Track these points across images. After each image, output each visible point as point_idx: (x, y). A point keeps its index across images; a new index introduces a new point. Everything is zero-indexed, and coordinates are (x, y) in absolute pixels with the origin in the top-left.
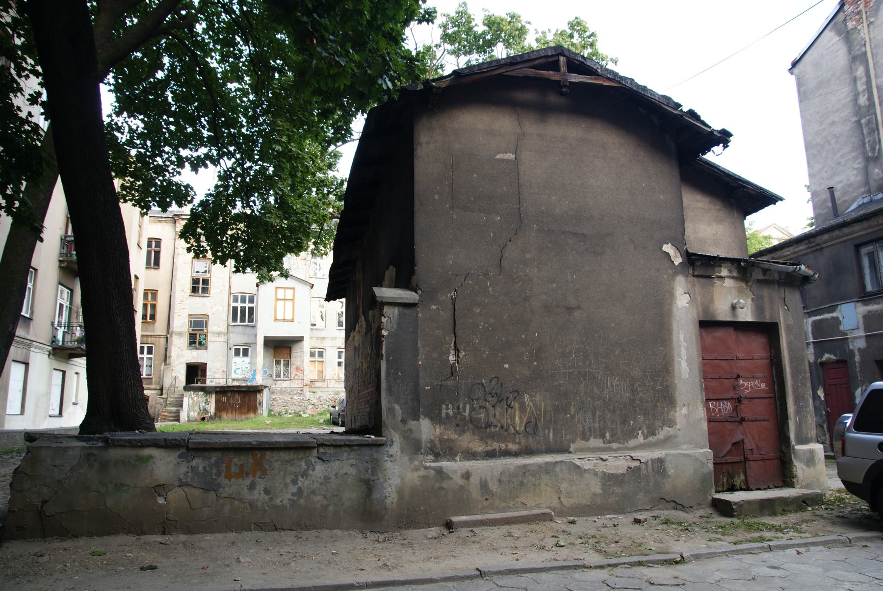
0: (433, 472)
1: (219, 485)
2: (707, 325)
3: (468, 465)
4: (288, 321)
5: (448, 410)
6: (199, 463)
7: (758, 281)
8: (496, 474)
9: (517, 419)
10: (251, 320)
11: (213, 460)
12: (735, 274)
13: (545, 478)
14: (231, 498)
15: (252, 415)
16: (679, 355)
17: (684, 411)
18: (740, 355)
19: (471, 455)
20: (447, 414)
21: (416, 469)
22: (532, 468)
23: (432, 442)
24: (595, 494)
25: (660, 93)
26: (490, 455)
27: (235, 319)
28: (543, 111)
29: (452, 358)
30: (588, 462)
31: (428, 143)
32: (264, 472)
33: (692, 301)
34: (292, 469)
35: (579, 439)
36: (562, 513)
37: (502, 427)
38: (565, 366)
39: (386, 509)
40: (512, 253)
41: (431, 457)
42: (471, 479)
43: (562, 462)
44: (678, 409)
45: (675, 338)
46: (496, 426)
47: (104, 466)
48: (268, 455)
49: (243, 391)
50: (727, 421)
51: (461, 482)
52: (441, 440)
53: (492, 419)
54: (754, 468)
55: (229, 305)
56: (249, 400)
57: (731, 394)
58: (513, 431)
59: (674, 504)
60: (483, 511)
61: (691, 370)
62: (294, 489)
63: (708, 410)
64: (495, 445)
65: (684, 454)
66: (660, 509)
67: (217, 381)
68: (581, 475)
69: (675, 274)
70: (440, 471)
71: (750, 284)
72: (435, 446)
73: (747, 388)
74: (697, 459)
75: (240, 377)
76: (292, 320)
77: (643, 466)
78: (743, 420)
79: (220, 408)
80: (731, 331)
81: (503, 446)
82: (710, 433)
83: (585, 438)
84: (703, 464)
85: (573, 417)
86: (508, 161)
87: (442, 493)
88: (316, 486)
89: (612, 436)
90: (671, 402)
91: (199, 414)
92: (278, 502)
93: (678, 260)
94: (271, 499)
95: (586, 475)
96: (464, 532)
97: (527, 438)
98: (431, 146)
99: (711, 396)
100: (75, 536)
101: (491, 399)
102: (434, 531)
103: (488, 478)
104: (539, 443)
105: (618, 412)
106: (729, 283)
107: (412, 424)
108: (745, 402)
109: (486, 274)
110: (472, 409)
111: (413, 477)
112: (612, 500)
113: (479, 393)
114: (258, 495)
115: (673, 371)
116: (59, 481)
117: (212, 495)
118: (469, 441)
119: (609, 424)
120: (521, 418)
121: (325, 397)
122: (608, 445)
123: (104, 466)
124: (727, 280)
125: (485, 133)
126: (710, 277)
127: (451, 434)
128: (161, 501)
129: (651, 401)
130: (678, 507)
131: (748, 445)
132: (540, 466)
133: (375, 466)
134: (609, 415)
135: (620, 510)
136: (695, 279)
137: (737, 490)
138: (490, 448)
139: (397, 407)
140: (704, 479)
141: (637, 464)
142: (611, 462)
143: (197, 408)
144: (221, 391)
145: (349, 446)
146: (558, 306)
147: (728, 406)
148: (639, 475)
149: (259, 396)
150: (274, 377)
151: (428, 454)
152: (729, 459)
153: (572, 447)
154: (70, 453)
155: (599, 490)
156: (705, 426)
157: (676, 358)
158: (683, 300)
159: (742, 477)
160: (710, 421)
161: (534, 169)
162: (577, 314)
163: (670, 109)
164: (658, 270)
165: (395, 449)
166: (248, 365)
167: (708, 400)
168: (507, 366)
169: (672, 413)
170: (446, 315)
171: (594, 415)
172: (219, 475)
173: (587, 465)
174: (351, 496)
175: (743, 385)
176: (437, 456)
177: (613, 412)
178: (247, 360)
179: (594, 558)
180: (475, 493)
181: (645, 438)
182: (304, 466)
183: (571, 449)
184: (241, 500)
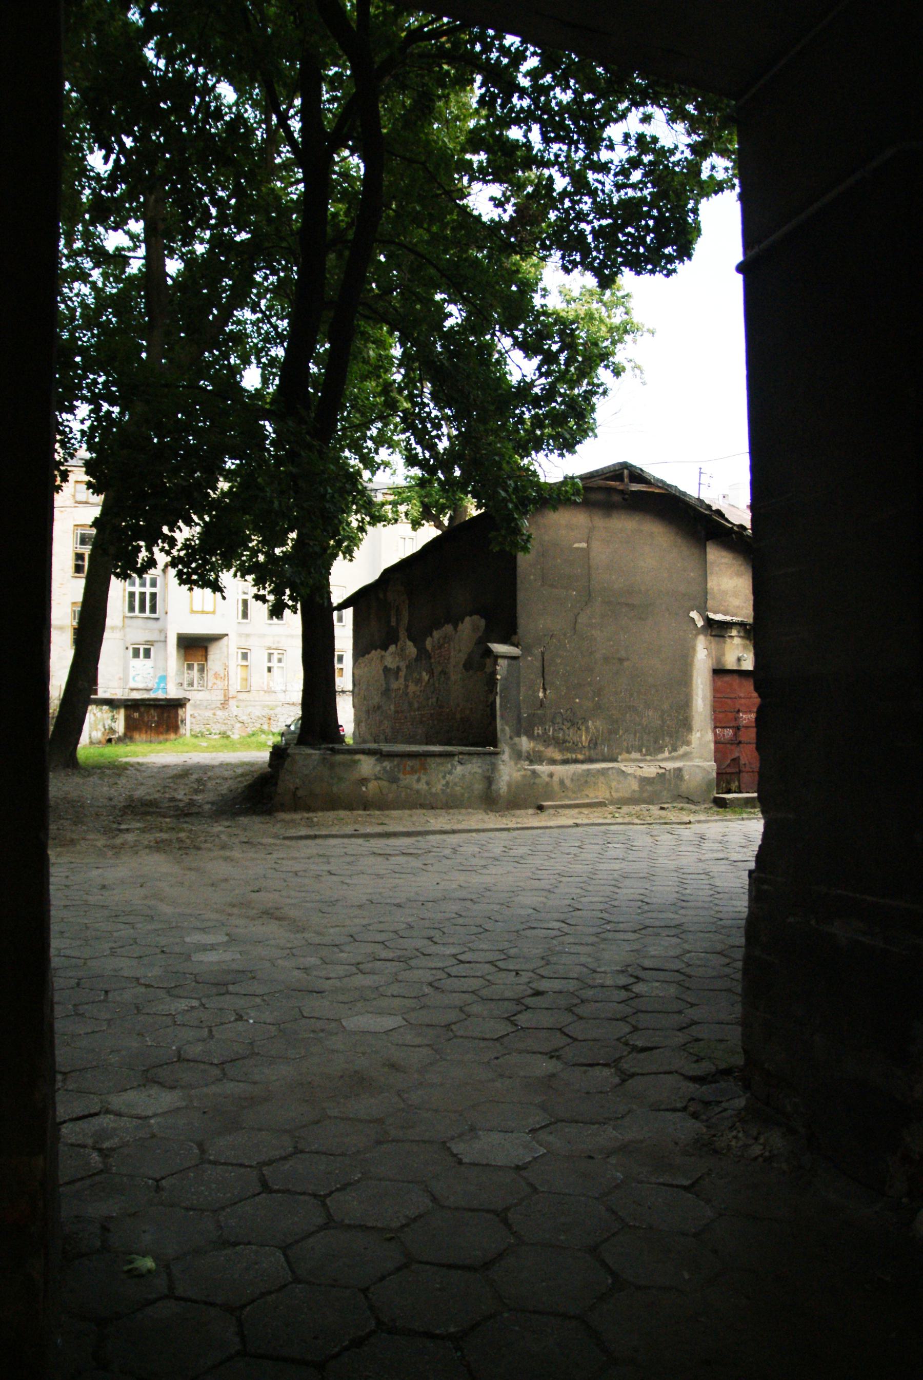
0: (529, 773)
1: (399, 779)
2: (719, 672)
3: (552, 768)
4: (208, 613)
5: (538, 731)
6: (387, 764)
8: (570, 773)
9: (584, 737)
10: (153, 609)
11: (395, 763)
12: (742, 634)
13: (601, 779)
15: (172, 736)
17: (698, 735)
18: (742, 695)
19: (553, 762)
21: (518, 771)
23: (528, 752)
24: (634, 791)
26: (566, 762)
27: (132, 608)
29: (541, 695)
30: (630, 768)
32: (425, 769)
33: (709, 655)
36: (612, 803)
41: (527, 763)
43: (612, 768)
45: (694, 682)
47: (332, 766)
48: (429, 760)
49: (161, 705)
51: (547, 779)
52: (534, 751)
53: (567, 737)
54: (746, 777)
55: (124, 590)
56: (169, 717)
60: (561, 799)
62: (444, 782)
63: (715, 734)
64: (569, 756)
67: (113, 691)
68: (625, 778)
69: (698, 634)
70: (534, 772)
75: (141, 686)
76: (214, 612)
78: (740, 742)
79: (132, 727)
81: (574, 756)
82: (716, 751)
83: (629, 752)
85: (621, 737)
86: (582, 549)
88: (457, 780)
89: (647, 751)
90: (689, 729)
91: (103, 734)
92: (434, 790)
93: (700, 623)
95: (629, 778)
99: (718, 723)
102: (531, 811)
106: (737, 641)
107: (516, 740)
108: (743, 729)
109: (565, 635)
110: (554, 730)
111: (517, 776)
112: (645, 795)
113: (559, 720)
114: (422, 786)
117: (394, 786)
121: (258, 714)
123: (332, 766)
124: (736, 639)
125: (566, 528)
126: (723, 637)
131: (742, 762)
132: (598, 771)
133: (494, 767)
134: (645, 737)
135: (650, 802)
136: (712, 638)
139: (507, 728)
140: (709, 785)
141: (663, 771)
143: (101, 727)
144: (132, 707)
149: (180, 712)
150: (185, 686)
151: (525, 760)
152: (729, 770)
153: (620, 758)
156: (712, 746)
157: (695, 697)
158: (702, 655)
159: (737, 783)
160: (716, 742)
161: (601, 553)
162: (626, 664)
165: (506, 757)
166: (151, 671)
167: (716, 727)
170: (538, 664)
171: (635, 735)
173: (629, 770)
174: (479, 787)
176: (532, 762)
178: (148, 663)
179: (639, 822)
180: (556, 787)
181: (670, 753)
184: (411, 789)
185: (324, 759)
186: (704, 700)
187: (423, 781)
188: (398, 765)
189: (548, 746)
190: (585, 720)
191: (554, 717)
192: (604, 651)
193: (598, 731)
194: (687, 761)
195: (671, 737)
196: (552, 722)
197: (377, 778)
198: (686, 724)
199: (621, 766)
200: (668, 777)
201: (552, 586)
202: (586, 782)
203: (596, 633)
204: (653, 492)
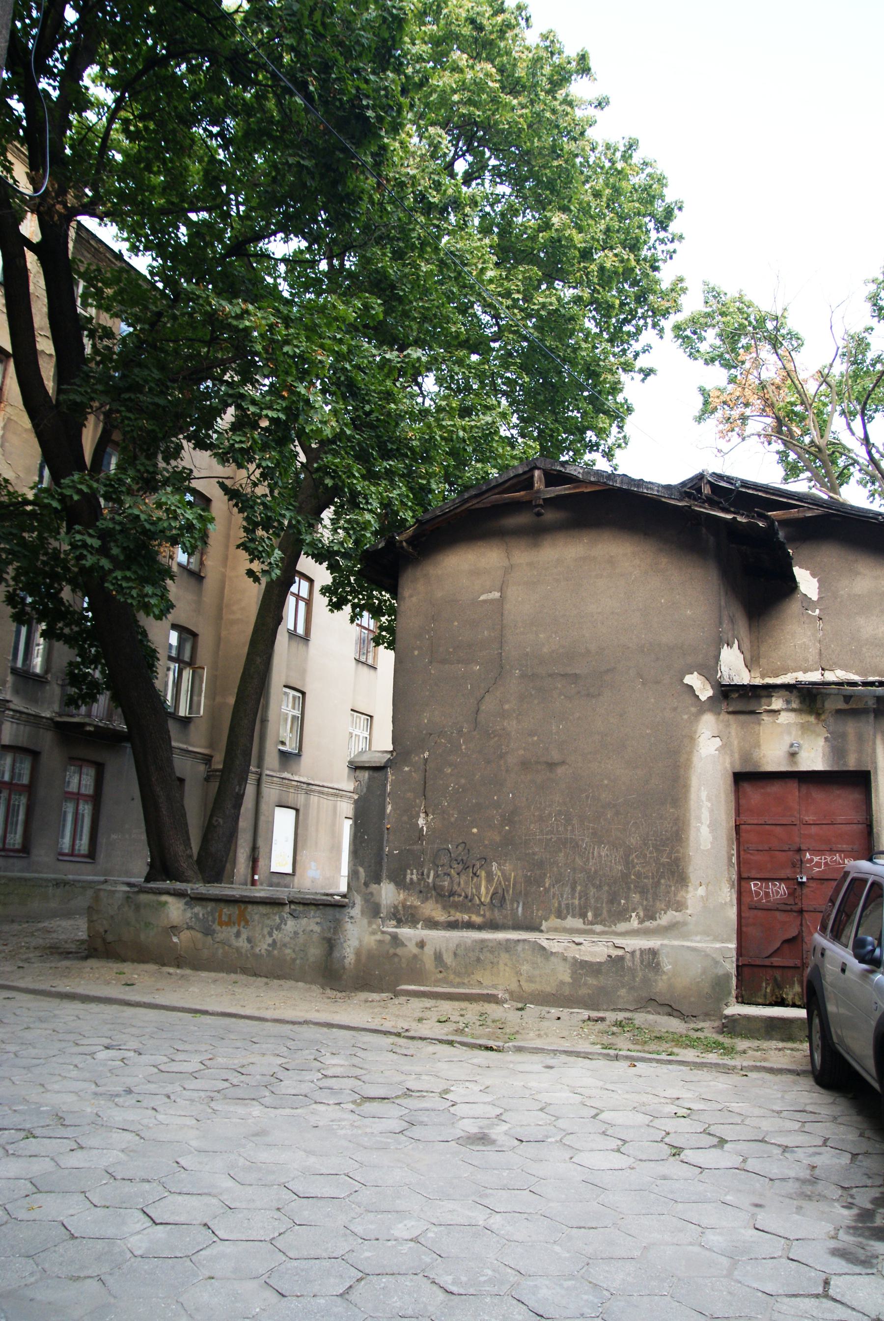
0: (388, 937)
2: (746, 779)
5: (412, 876)
6: (198, 909)
7: (839, 712)
8: (452, 946)
11: (209, 909)
13: (504, 956)
14: (222, 943)
16: (699, 819)
17: (701, 891)
18: (809, 818)
19: (432, 924)
20: (411, 879)
21: (374, 933)
22: (490, 944)
23: (395, 907)
24: (562, 983)
25: (675, 479)
26: (453, 925)
28: (536, 533)
31: (411, 596)
32: (247, 922)
33: (725, 747)
34: (268, 922)
35: (553, 917)
37: (466, 897)
38: (542, 831)
39: (344, 968)
40: (489, 705)
42: (426, 949)
43: (524, 940)
44: (690, 889)
45: (693, 795)
46: (460, 895)
47: (138, 908)
48: (250, 907)
50: (777, 910)
51: (415, 950)
53: (456, 887)
57: (787, 872)
58: (478, 902)
59: (669, 1010)
60: (437, 982)
61: (715, 838)
62: (269, 940)
65: (688, 947)
66: (649, 1012)
70: (395, 937)
71: (823, 717)
72: (398, 911)
73: (818, 865)
74: (707, 955)
77: (628, 956)
80: (793, 787)
81: (466, 917)
83: (560, 916)
84: (717, 963)
85: (547, 890)
87: (396, 960)
88: (287, 939)
89: (595, 916)
92: (257, 950)
93: (705, 692)
94: (252, 947)
96: (402, 999)
97: (493, 910)
98: (414, 599)
100: (124, 960)
101: (456, 866)
103: (443, 950)
104: (505, 917)
105: (606, 888)
106: (786, 718)
107: (374, 887)
109: (460, 731)
110: (437, 876)
112: (583, 991)
113: (444, 860)
114: (242, 943)
115: (688, 839)
116: (112, 917)
118: (433, 910)
119: (592, 901)
120: (487, 889)
122: (590, 927)
123: (138, 908)
124: (783, 714)
126: (753, 712)
127: (414, 901)
128: (175, 939)
129: (658, 874)
130: (675, 1013)
133: (337, 926)
134: (592, 891)
137: (787, 1006)
138: (452, 918)
139: (361, 870)
141: (620, 952)
142: (587, 947)
145: (316, 905)
146: (537, 763)
147: (782, 889)
148: (623, 967)
152: (776, 961)
153: (544, 925)
154: (117, 895)
155: (567, 979)
157: (693, 823)
161: (521, 603)
162: (560, 770)
163: (673, 502)
164: (675, 709)
168: (475, 830)
169: (683, 893)
170: (417, 777)
171: (573, 889)
172: (213, 922)
174: (315, 952)
175: (811, 860)
176: (400, 923)
177: (599, 887)
180: (429, 963)
181: (641, 922)
182: (278, 920)
183: (543, 928)
184: (230, 946)
185: (128, 897)
186: (713, 826)
187: (244, 936)
188: (212, 913)
189: (425, 900)
190: (485, 860)
191: (436, 856)
192: (521, 752)
193: (507, 879)
194: (676, 938)
195: (643, 892)
196: (434, 863)
197: (189, 928)
198: (675, 872)
199: (541, 939)
200: (628, 963)
201: (443, 662)
202: (478, 960)
203: (511, 725)
204: (583, 493)
